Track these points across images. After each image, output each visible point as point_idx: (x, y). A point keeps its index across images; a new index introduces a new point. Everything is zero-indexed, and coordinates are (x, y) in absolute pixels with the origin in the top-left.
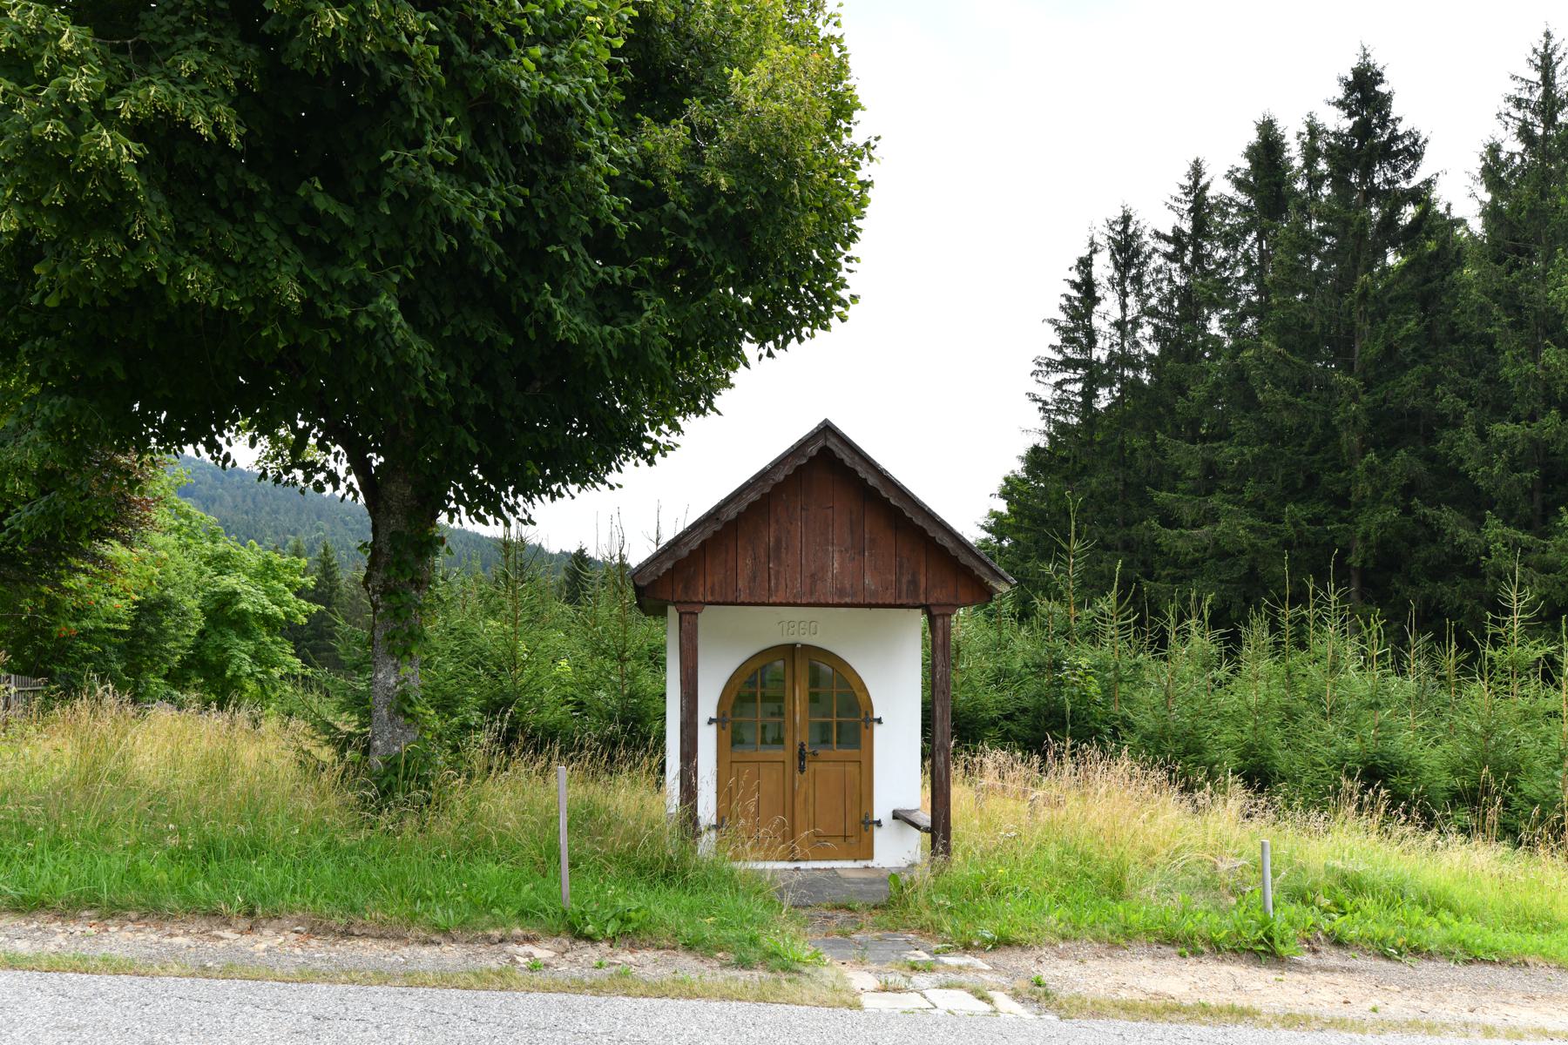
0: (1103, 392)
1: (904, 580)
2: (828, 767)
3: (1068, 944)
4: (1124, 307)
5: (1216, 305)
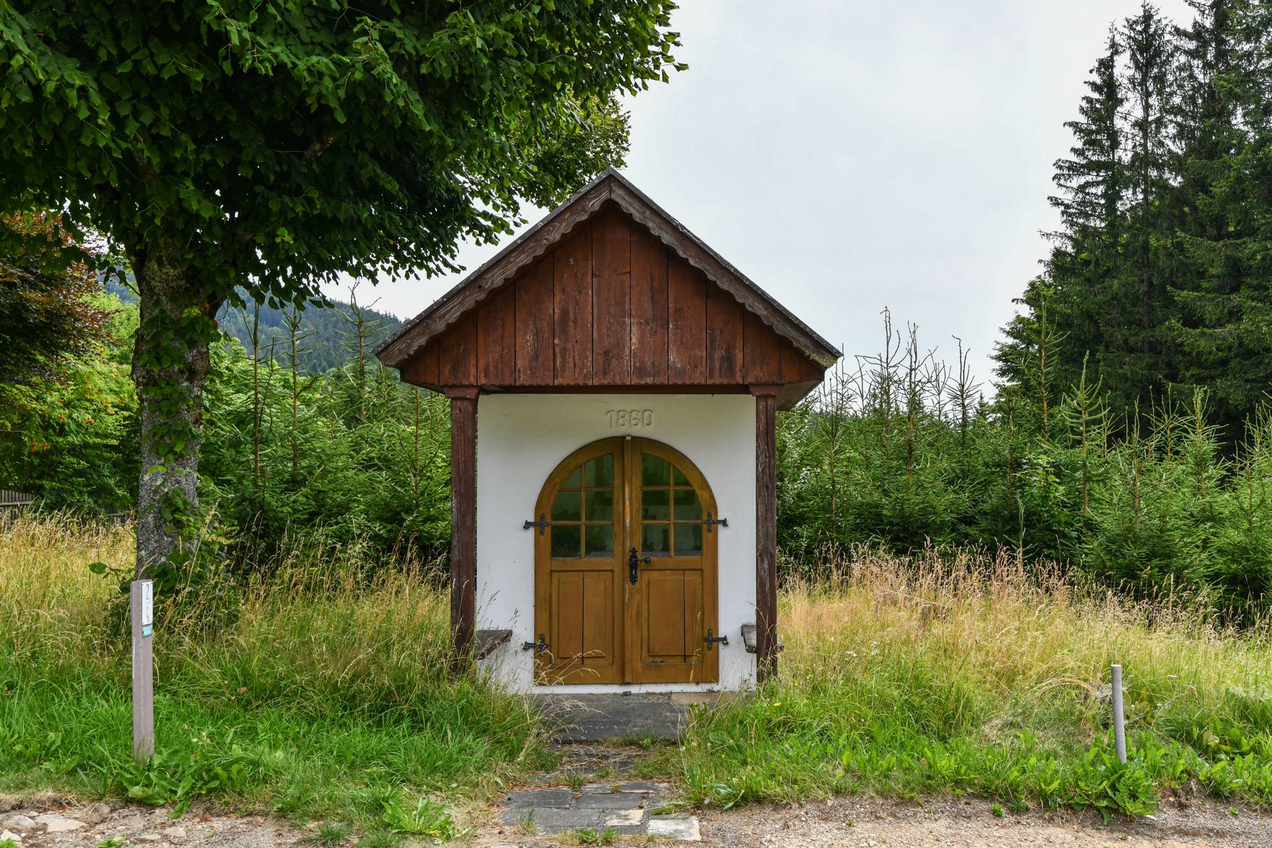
0: (1127, 194)
1: (718, 354)
2: (662, 578)
3: (841, 800)
4: (1147, 107)
5: (1242, 99)
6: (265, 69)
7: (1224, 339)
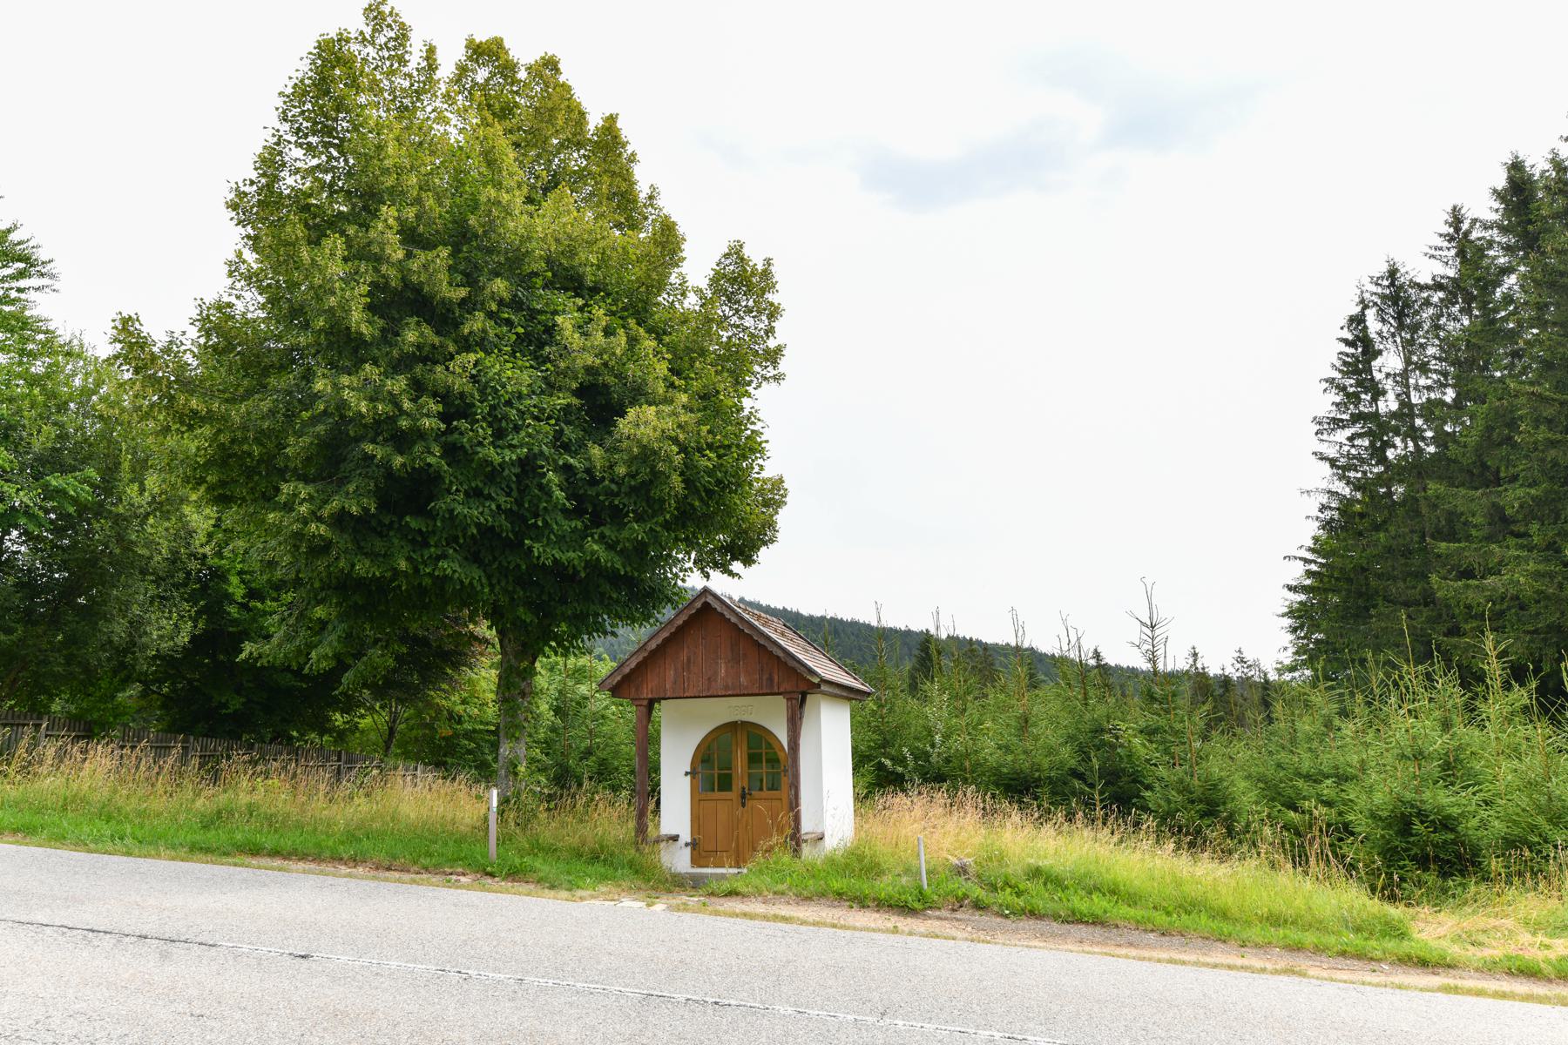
6: (549, 562)
7: (1494, 589)
